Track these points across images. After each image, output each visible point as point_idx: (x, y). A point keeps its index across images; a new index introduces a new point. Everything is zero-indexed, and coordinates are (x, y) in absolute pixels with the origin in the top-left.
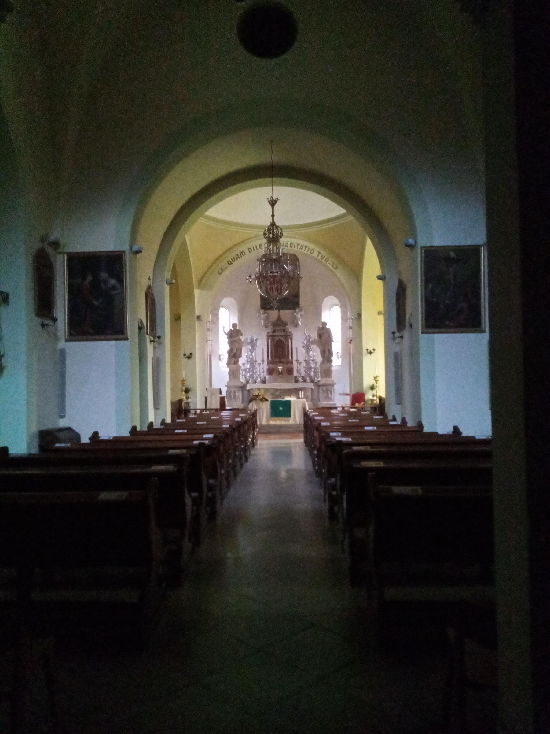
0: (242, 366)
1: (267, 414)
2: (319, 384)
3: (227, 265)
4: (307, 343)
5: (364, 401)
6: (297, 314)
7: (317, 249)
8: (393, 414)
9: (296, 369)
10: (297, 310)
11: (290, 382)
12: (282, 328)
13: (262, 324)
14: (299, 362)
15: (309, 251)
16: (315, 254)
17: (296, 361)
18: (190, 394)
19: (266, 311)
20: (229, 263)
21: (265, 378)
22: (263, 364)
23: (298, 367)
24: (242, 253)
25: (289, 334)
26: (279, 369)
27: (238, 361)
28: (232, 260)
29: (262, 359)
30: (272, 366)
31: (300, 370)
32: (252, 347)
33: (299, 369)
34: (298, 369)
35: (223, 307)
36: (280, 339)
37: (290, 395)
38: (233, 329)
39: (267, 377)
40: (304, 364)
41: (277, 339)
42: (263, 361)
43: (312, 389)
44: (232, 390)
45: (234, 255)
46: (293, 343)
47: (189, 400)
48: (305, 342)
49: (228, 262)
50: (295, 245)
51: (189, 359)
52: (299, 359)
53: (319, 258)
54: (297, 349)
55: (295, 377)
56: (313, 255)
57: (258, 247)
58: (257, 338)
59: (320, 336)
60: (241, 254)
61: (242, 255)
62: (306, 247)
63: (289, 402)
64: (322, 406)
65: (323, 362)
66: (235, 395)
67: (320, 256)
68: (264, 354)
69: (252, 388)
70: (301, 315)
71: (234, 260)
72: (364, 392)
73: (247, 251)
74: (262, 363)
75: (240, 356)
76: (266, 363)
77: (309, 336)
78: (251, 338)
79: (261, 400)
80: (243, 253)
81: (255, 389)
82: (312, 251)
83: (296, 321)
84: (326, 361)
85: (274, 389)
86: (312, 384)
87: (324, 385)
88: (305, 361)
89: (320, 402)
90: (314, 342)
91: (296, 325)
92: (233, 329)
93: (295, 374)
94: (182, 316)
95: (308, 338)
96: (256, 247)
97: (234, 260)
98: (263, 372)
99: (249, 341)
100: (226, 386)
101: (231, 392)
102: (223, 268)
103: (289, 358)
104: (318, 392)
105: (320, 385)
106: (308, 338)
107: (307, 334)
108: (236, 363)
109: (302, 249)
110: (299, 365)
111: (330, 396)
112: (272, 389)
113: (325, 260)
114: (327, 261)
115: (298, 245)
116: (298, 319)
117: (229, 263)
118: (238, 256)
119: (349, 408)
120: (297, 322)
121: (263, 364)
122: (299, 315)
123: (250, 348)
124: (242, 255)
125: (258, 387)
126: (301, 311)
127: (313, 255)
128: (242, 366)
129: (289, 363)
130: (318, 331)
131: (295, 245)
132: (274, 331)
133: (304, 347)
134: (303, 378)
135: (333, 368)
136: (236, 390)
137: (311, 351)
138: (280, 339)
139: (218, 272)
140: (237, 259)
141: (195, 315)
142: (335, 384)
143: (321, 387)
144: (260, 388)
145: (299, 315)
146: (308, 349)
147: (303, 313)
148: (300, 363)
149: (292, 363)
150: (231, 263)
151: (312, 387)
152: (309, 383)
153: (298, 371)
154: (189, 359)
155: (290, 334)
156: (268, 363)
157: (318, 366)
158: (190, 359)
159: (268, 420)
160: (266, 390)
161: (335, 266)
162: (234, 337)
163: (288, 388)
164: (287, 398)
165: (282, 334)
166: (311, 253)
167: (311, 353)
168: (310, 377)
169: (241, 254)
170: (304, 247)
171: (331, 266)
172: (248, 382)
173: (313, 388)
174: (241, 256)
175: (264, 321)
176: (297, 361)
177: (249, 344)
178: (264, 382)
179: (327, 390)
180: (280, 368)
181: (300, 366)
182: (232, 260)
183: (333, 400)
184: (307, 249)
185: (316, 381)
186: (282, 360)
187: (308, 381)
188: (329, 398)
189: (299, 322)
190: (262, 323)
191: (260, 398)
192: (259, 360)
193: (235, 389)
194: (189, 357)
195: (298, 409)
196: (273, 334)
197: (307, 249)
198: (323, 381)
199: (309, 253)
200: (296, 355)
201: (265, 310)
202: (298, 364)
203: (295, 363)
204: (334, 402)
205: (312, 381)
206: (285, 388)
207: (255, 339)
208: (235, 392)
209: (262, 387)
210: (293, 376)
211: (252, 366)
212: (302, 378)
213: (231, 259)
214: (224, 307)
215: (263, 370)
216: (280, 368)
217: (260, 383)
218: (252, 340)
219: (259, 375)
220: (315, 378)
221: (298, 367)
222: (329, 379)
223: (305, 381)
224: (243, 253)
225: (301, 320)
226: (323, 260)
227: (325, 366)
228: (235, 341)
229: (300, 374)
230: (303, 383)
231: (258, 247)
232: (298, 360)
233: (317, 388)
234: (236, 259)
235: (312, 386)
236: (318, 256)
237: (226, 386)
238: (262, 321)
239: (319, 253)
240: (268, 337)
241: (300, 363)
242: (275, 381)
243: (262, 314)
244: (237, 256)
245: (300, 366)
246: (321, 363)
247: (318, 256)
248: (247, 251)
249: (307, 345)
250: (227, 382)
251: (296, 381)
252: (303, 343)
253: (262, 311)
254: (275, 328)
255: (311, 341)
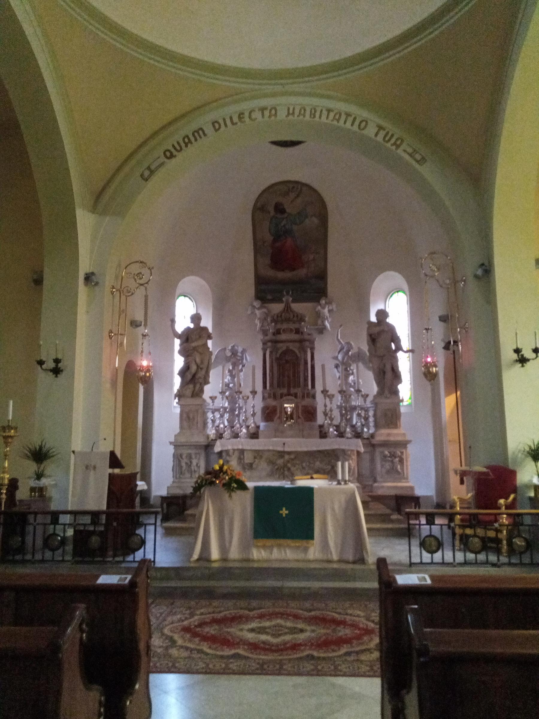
0: (209, 401)
1: (243, 526)
2: (374, 441)
3: (163, 159)
4: (343, 359)
5: (515, 490)
6: (324, 308)
7: (374, 119)
8: (462, 486)
9: (323, 409)
10: (323, 302)
11: (309, 436)
12: (292, 326)
13: (258, 328)
14: (329, 393)
15: (357, 123)
16: (370, 131)
17: (322, 392)
18: (49, 467)
19: (266, 305)
20: (168, 154)
21: (258, 427)
22: (254, 397)
23: (325, 406)
24: (199, 133)
25: (306, 337)
26: (285, 408)
27: (202, 391)
28: (175, 149)
29: (251, 389)
30: (272, 403)
31: (331, 410)
32: (234, 365)
33: (328, 408)
34: (326, 410)
35: (185, 296)
36: (287, 347)
37: (310, 474)
38: (192, 326)
39: (262, 425)
40: (338, 399)
41: (283, 347)
42: (254, 393)
43: (358, 453)
44: (185, 452)
45: (178, 137)
46: (316, 357)
47: (44, 481)
48: (340, 357)
49: (164, 153)
50: (321, 111)
51: (56, 376)
52: (327, 389)
53: (380, 138)
54: (323, 366)
55: (321, 426)
56: (365, 132)
57: (235, 119)
58: (243, 349)
59: (373, 339)
60: (196, 134)
61: (198, 138)
62: (348, 115)
63: (310, 491)
64: (380, 492)
65: (380, 393)
66: (189, 465)
67: (382, 134)
68: (256, 377)
69: (226, 448)
70: (330, 311)
71: (178, 148)
72: (511, 467)
73: (209, 129)
74: (251, 396)
75: (207, 382)
76: (259, 396)
77: (348, 343)
78: (233, 347)
79: (227, 486)
80: (201, 132)
81: (234, 450)
82: (364, 124)
83: (320, 322)
84: (386, 392)
85: (273, 451)
86: (359, 442)
87: (385, 444)
88: (340, 392)
89: (375, 481)
90: (359, 357)
91: (322, 330)
92: (192, 326)
93: (320, 419)
94: (47, 272)
95: (346, 349)
96: (231, 118)
97: (178, 148)
98: (254, 415)
99: (229, 354)
100: (171, 443)
101: (181, 456)
102: (153, 167)
103: (306, 385)
104: (372, 461)
105: (375, 443)
106: (345, 350)
107: (342, 342)
108: (198, 393)
109: (338, 121)
110: (328, 400)
111: (399, 470)
112: (269, 451)
113: (395, 144)
114: (398, 147)
115: (329, 111)
116: (324, 319)
117: (168, 154)
118: (189, 139)
119: (224, 396)
120: (323, 322)
121: (254, 397)
122: (326, 311)
123: (231, 368)
124: (198, 138)
125: (240, 447)
126: (329, 303)
127: (365, 132)
128: (209, 401)
129: (308, 396)
130: (368, 329)
131: (321, 111)
132: (278, 332)
133: (337, 366)
134: (337, 428)
135: (402, 410)
136: (192, 452)
137: (353, 374)
138: (287, 347)
139: (142, 175)
140: (186, 146)
141: (77, 271)
142: (409, 442)
143: (378, 450)
144: (245, 448)
145: (326, 311)
146: (346, 369)
147: (334, 306)
148: (331, 397)
149: (314, 397)
150: (172, 156)
151: (359, 449)
152: (350, 438)
153: (325, 414)
154: (56, 376)
155: (309, 337)
156: (264, 398)
157: (368, 404)
158: (58, 375)
159: (245, 547)
160: (258, 454)
161: (418, 157)
162: (193, 342)
163: (305, 449)
164: (303, 482)
165: (296, 337)
166: (359, 128)
167: (351, 378)
168: (353, 427)
169: (196, 134)
170: (343, 117)
171: (407, 157)
172: (220, 436)
173: (362, 450)
174: (196, 140)
175: (260, 323)
176: (325, 392)
177: (228, 359)
178: (254, 435)
179: (393, 456)
180: (289, 407)
181: (331, 403)
182: (175, 149)
183: (406, 479)
184: (350, 120)
185: (365, 436)
186: (293, 391)
187: (349, 435)
188: (397, 471)
189: (327, 323)
190: (257, 325)
191: (224, 481)
192: (247, 391)
193: (189, 451)
194: (56, 371)
195: (334, 515)
196: (274, 338)
197: (350, 120)
198: (383, 434)
199: (355, 128)
200: (321, 370)
201: (263, 303)
202: (325, 399)
203: (319, 397)
204: (408, 482)
205: (358, 435)
206: (299, 449)
207: (240, 349)
208: (190, 457)
209: (248, 448)
210: (313, 423)
211: (232, 400)
212: (335, 428)
213: (173, 146)
214: (187, 297)
215: (253, 411)
216: (289, 407)
217: (246, 438)
218: (234, 353)
219: (243, 420)
220: (363, 429)
221: (325, 406)
222: (395, 431)
223: (341, 435)
224: (201, 132)
225: (330, 320)
226: (389, 145)
227: (386, 402)
228: (195, 349)
229: (332, 419)
230: (339, 439)
231: (235, 119)
232: (327, 391)
233: (370, 449)
234: (183, 145)
235: (359, 445)
236: (376, 135)
237: (171, 443)
238: (257, 322)
239: (380, 128)
240: (264, 344)
241: (331, 397)
242: (278, 433)
243: (258, 309)
244: (186, 140)
245: (331, 403)
246: (375, 397)
247: (376, 135)
248: (209, 129)
249: (343, 363)
250: (175, 436)
251: (323, 435)
252: (336, 358)
253: (257, 304)
254: (279, 326)
255: (352, 354)
